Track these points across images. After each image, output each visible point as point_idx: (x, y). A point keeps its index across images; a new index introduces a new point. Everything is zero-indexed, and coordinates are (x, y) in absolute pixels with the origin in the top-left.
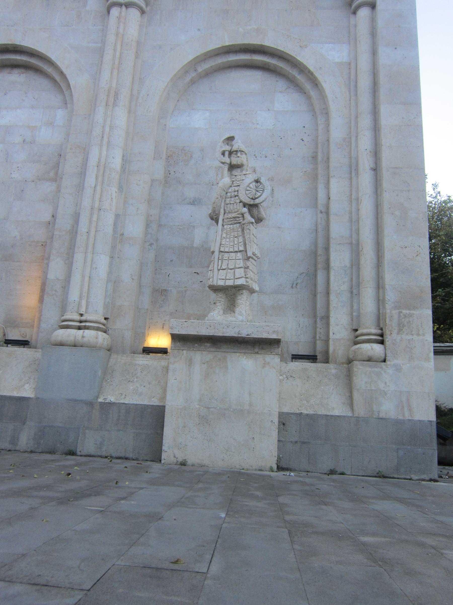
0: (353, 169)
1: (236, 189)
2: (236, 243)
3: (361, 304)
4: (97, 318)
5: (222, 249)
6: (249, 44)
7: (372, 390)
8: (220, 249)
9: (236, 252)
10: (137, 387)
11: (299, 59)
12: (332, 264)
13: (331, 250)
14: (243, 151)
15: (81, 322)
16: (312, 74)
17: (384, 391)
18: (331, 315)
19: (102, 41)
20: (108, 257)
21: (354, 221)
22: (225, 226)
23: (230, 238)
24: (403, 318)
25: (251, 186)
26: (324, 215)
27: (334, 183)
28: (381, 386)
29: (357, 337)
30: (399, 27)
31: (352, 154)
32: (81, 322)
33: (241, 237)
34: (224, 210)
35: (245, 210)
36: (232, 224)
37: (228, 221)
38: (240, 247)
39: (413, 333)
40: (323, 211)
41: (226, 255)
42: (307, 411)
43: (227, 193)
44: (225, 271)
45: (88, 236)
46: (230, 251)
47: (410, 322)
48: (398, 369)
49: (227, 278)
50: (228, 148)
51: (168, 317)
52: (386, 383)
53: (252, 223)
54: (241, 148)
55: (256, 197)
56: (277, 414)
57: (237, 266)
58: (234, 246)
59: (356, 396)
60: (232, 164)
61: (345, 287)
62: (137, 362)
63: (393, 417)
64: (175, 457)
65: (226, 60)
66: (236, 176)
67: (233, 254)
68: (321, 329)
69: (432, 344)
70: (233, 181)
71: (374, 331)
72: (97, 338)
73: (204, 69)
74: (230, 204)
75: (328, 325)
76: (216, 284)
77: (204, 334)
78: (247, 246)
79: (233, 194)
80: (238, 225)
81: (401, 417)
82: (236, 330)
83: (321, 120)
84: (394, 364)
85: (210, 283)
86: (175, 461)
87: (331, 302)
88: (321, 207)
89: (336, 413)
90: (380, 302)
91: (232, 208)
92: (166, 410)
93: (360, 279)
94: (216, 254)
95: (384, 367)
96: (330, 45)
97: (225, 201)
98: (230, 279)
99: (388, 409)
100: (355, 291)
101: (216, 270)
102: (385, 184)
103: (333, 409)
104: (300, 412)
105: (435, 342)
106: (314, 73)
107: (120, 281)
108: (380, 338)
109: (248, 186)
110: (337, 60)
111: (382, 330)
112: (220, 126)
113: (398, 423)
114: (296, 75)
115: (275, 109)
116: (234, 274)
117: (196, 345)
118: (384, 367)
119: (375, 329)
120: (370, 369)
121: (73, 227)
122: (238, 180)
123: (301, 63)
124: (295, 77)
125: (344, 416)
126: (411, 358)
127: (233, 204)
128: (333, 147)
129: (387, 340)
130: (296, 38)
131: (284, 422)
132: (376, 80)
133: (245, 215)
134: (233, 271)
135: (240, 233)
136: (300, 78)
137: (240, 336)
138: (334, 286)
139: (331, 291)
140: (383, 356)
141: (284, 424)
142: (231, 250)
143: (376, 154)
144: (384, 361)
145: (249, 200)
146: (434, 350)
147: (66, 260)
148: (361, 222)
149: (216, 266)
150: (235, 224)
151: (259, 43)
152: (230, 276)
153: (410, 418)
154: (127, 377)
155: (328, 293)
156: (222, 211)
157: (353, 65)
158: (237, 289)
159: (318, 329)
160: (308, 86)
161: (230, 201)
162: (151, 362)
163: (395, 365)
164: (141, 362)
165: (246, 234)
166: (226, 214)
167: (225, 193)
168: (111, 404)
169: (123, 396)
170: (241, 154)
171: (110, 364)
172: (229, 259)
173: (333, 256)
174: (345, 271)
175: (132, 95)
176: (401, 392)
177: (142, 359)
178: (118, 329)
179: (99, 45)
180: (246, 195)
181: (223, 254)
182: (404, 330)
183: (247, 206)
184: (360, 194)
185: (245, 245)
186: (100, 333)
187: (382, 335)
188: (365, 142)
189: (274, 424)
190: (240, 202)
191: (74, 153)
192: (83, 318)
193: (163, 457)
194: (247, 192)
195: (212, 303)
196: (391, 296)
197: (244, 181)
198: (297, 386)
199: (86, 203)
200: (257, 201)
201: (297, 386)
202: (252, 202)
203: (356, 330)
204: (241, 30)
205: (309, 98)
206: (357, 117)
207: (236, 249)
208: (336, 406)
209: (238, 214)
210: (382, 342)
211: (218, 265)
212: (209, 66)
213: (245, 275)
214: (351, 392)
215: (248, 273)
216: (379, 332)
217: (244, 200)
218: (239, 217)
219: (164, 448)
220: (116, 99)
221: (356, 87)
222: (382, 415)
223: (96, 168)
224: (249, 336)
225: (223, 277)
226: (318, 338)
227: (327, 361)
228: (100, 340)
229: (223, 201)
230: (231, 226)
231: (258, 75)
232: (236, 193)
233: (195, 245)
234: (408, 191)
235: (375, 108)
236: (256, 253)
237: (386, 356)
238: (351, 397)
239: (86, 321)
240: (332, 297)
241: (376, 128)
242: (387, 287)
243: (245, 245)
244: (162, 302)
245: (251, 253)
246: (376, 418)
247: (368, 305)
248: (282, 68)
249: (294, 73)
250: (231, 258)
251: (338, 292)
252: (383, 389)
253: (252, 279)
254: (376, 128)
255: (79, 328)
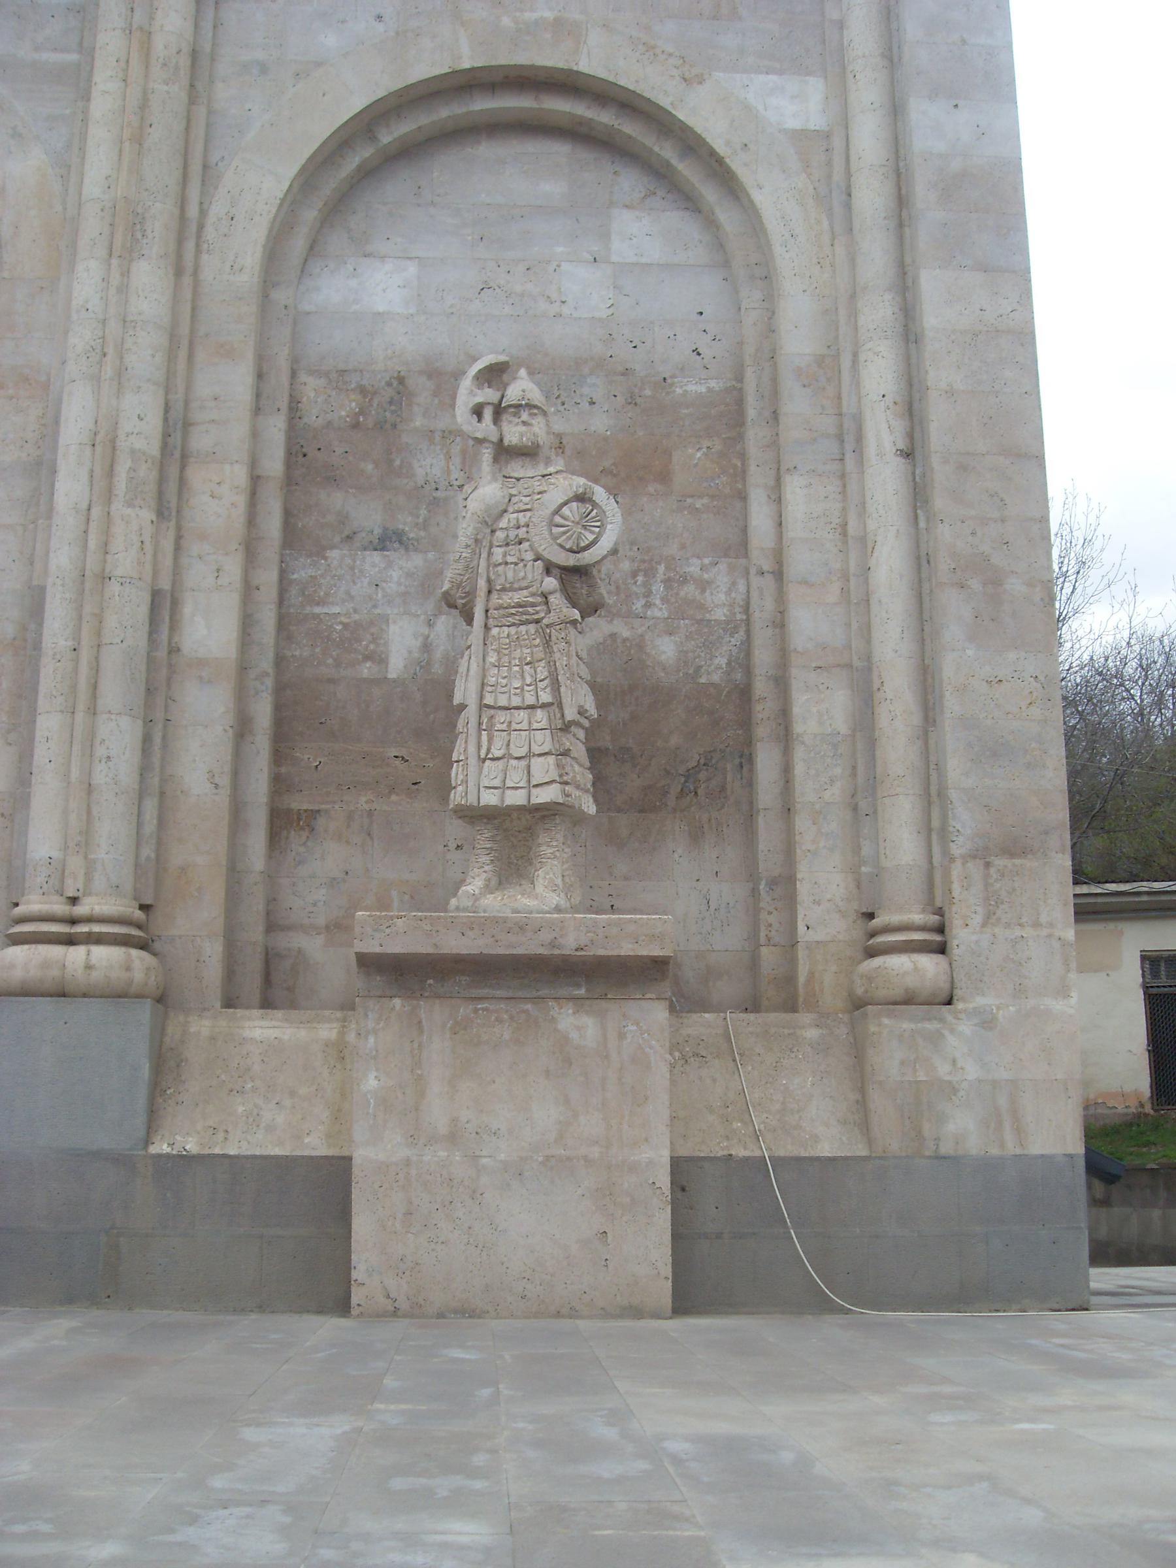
0: (848, 438)
1: (523, 518)
2: (529, 680)
3: (881, 842)
4: (121, 909)
5: (489, 700)
6: (532, 67)
7: (917, 1082)
8: (482, 698)
9: (532, 707)
10: (256, 1106)
11: (681, 116)
12: (798, 728)
13: (796, 686)
14: (535, 407)
15: (73, 921)
16: (720, 161)
17: (950, 1082)
18: (799, 876)
19: (81, 44)
20: (140, 722)
21: (858, 602)
22: (495, 631)
23: (509, 667)
24: (996, 880)
25: (566, 511)
26: (768, 582)
27: (795, 490)
28: (943, 1070)
29: (873, 935)
30: (964, 42)
31: (845, 403)
32: (73, 921)
33: (542, 664)
34: (489, 581)
35: (551, 583)
36: (513, 625)
37: (504, 616)
38: (540, 693)
39: (1024, 920)
40: (766, 568)
41: (501, 716)
42: (745, 1149)
43: (493, 531)
44: (500, 764)
45: (76, 661)
46: (514, 704)
47: (1014, 890)
48: (987, 1022)
49: (509, 784)
50: (489, 395)
51: (323, 891)
52: (954, 1061)
53: (574, 623)
54: (529, 395)
55: (582, 544)
56: (666, 1161)
57: (536, 749)
58: (522, 689)
59: (878, 1101)
60: (506, 442)
61: (835, 793)
62: (247, 1033)
63: (974, 1152)
64: (388, 1297)
65: (464, 110)
66: (518, 479)
67: (522, 713)
68: (770, 913)
69: (1071, 890)
70: (511, 496)
71: (918, 918)
72: (128, 969)
73: (396, 135)
74: (506, 563)
75: (790, 900)
76: (476, 804)
77: (454, 951)
78: (562, 689)
79: (512, 534)
80: (532, 628)
81: (995, 1151)
82: (545, 936)
83: (751, 297)
84: (974, 1009)
85: (458, 799)
86: (391, 1308)
87: (797, 838)
88: (760, 558)
89: (825, 1150)
90: (934, 837)
91: (510, 575)
92: (356, 1171)
93: (879, 770)
94: (471, 712)
95: (950, 1018)
96: (771, 77)
97: (490, 554)
98: (517, 788)
99: (963, 1129)
100: (862, 805)
101: (473, 761)
102: (940, 502)
103: (816, 1139)
104: (726, 1153)
105: (1076, 882)
106: (727, 160)
107: (179, 793)
108: (937, 938)
109: (557, 512)
110: (792, 124)
111: (942, 916)
112: (452, 306)
113: (988, 1167)
114: (674, 162)
115: (615, 258)
116: (529, 772)
117: (431, 981)
118: (950, 1018)
119: (923, 911)
120: (913, 1026)
121: (24, 628)
122: (525, 492)
123: (685, 129)
124: (668, 164)
125: (846, 1158)
126: (1020, 991)
127: (516, 564)
128: (790, 385)
129: (955, 942)
130: (670, 55)
131: (685, 1183)
132: (903, 192)
133: (552, 599)
134: (523, 763)
135: (539, 653)
136: (685, 169)
137: (556, 952)
138: (806, 789)
139: (798, 806)
140: (947, 986)
141: (683, 1189)
142: (516, 701)
143: (912, 408)
144: (949, 1002)
145: (564, 554)
146: (1075, 904)
147: (9, 732)
148: (875, 608)
149: (472, 749)
150: (523, 623)
151: (561, 65)
152: (516, 777)
153: (1018, 1151)
154: (223, 1077)
155: (788, 811)
156: (482, 584)
157: (837, 143)
158: (538, 815)
159: (763, 916)
160: (709, 194)
161: (505, 555)
162: (289, 1031)
163: (977, 1011)
164: (257, 1034)
165: (557, 655)
166: (494, 595)
167: (488, 531)
168: (186, 1160)
169: (221, 1136)
170: (530, 414)
171: (167, 1039)
172: (509, 730)
173: (801, 702)
174: (835, 746)
175: (183, 218)
176: (995, 1084)
177: (263, 1023)
178: (180, 937)
179: (73, 57)
180: (555, 538)
181: (492, 712)
182: (999, 913)
183: (556, 571)
184: (871, 525)
185: (556, 686)
186: (135, 953)
187: (941, 929)
188: (879, 375)
189: (658, 1191)
190: (535, 560)
191: (11, 398)
192: (81, 910)
193: (354, 1300)
194: (556, 530)
195: (452, 846)
196: (965, 823)
197: (546, 497)
198: (714, 1080)
199: (62, 557)
200: (587, 557)
201: (714, 1080)
202: (571, 560)
203: (871, 916)
204: (506, 21)
205: (711, 223)
206: (853, 297)
207: (530, 700)
208: (824, 1133)
209: (533, 595)
210: (942, 949)
211: (479, 747)
212: (414, 126)
213: (561, 776)
214: (862, 1090)
215: (568, 769)
216: (934, 919)
217: (546, 555)
218: (533, 605)
219: (355, 1275)
220: (139, 235)
221: (848, 206)
222: (946, 1148)
223: (88, 450)
224: (583, 953)
225: (497, 783)
226: (763, 940)
227: (791, 1006)
228: (138, 975)
229: (484, 555)
230: (513, 630)
231: (559, 150)
232: (522, 532)
233: (392, 675)
234: (1003, 521)
235: (905, 274)
236: (587, 707)
237: (952, 987)
238: (862, 1104)
239: (90, 920)
240: (802, 823)
241: (909, 333)
242: (953, 794)
243: (556, 686)
244: (302, 849)
245: (575, 710)
246: (929, 1157)
247: (902, 844)
248: (630, 137)
249: (667, 151)
250: (518, 727)
251: (817, 807)
252: (947, 1078)
253: (578, 787)
254: (909, 333)
255: (70, 941)
